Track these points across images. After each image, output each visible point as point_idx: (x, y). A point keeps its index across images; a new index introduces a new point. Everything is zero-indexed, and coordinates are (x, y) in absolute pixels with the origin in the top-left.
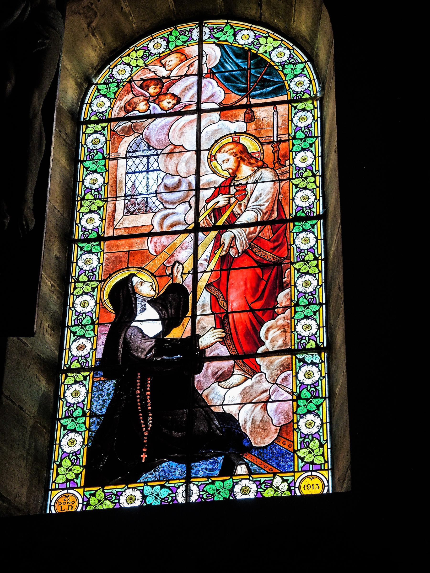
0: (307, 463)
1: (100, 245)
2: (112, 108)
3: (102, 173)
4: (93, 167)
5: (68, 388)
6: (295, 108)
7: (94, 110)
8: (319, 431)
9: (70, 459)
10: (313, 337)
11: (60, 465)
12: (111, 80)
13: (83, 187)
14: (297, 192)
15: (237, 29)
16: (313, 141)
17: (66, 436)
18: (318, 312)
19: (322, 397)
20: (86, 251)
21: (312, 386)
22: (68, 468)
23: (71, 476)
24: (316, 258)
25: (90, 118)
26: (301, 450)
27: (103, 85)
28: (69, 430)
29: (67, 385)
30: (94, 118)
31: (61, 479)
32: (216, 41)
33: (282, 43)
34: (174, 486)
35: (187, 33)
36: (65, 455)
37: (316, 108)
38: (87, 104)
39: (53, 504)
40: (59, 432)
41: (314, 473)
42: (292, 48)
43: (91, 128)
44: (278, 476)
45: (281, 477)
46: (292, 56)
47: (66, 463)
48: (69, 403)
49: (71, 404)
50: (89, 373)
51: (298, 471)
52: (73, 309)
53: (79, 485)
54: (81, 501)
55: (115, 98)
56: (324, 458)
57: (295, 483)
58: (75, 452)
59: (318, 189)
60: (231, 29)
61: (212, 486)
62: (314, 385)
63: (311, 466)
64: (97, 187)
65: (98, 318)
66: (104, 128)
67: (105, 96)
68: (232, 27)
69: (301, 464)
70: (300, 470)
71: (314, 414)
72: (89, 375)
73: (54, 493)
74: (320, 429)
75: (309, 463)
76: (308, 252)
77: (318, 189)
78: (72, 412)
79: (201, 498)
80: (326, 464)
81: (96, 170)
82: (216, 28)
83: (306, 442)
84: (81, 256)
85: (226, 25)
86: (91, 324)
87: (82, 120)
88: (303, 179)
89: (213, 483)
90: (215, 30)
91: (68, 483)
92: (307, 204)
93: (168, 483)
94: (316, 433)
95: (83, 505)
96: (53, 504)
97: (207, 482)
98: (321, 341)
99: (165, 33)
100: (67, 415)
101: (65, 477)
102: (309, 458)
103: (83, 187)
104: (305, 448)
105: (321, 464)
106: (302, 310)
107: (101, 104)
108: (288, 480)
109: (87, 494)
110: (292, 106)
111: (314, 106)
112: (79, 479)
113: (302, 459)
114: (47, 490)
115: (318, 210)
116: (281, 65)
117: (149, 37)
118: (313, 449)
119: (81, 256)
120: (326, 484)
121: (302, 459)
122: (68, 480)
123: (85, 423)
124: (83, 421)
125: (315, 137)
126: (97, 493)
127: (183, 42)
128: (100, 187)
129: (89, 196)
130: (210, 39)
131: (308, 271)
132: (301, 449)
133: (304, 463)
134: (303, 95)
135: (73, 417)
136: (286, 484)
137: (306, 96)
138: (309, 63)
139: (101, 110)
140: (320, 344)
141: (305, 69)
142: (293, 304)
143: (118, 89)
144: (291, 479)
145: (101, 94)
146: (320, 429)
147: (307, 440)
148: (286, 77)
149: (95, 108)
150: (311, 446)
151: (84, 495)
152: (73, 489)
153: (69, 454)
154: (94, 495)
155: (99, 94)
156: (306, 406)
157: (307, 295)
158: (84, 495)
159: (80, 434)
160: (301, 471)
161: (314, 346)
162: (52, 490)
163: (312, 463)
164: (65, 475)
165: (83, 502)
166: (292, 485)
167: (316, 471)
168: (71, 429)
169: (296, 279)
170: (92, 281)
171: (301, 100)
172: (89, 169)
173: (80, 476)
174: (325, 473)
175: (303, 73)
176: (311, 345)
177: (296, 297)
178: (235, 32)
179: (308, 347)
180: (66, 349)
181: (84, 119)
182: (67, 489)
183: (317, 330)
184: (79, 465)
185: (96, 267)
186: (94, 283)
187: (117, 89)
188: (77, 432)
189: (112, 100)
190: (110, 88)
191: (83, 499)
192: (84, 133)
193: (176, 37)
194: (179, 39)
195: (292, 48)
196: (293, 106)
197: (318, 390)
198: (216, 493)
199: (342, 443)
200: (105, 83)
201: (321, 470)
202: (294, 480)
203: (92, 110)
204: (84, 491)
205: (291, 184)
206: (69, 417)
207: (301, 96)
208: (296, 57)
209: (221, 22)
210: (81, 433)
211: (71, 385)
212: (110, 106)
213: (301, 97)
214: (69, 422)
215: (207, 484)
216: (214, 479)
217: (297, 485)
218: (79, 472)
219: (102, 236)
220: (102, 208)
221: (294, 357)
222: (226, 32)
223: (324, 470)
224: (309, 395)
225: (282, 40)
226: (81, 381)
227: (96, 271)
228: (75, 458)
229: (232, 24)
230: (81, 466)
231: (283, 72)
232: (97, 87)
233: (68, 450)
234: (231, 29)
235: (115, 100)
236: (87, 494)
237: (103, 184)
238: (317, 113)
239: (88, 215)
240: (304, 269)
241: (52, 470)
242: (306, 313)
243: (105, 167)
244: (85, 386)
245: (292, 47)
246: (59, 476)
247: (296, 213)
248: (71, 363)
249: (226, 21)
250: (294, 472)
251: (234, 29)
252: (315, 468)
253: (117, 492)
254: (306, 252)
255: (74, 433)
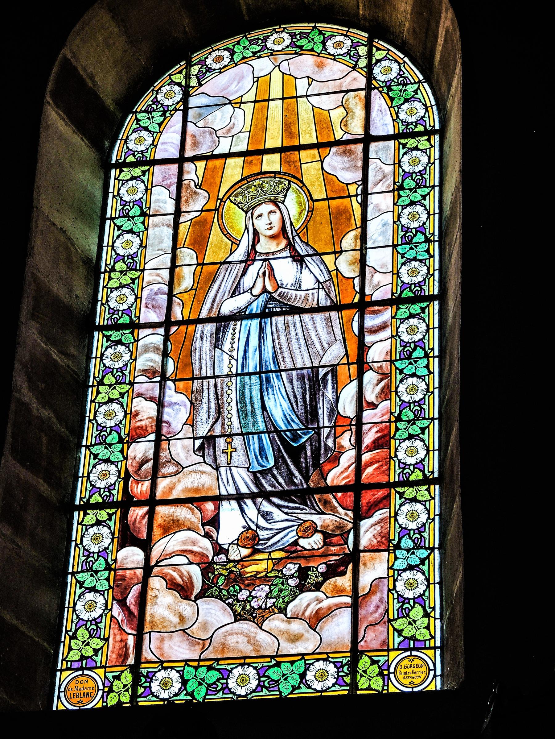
0: (406, 638)
1: (132, 333)
2: (156, 146)
3: (118, 462)
4: (90, 582)
5: (123, 184)
6: (401, 495)
7: (130, 148)
8: (424, 338)
9: (87, 629)
10: (421, 122)
11: (74, 637)
12: (154, 106)
13: (102, 365)
14: (401, 505)
15: (328, 34)
16: (426, 425)
17: (82, 597)
18: (427, 561)
19: (429, 419)
20: (102, 460)
21: (416, 531)
22: (85, 641)
23: (88, 652)
24: (427, 356)
25: (125, 159)
26: (399, 621)
27: (144, 114)
28: (86, 588)
29: (123, 180)
30: (131, 159)
31: (74, 656)
32: (298, 50)
33: (387, 54)
34: (226, 669)
35: (260, 41)
36: (82, 623)
37: (432, 146)
38: (96, 358)
39: (62, 689)
40: (72, 590)
41: (414, 653)
42: (402, 62)
43: (126, 174)
44: (366, 655)
45: (370, 657)
46: (401, 73)
47: (83, 634)
48: (125, 201)
49: (127, 202)
50: (114, 510)
51: (394, 650)
52: (94, 422)
53: (99, 665)
54: (101, 687)
55: (160, 132)
56: (430, 493)
57: (389, 667)
58: (95, 619)
59: (432, 149)
60: (319, 34)
61: (276, 669)
62: (419, 530)
63: (412, 642)
64: (121, 365)
65: (128, 435)
66: (144, 173)
67: (146, 129)
68: (320, 33)
69: (398, 640)
70: (396, 647)
71: (419, 319)
72: (115, 513)
73: (65, 674)
74: (424, 336)
75: (410, 639)
76: (414, 603)
77: (432, 149)
78: (104, 437)
79: (261, 686)
80: (432, 641)
81: (121, 339)
82: (299, 34)
83: (405, 609)
84: (94, 467)
85: (312, 30)
86: (118, 443)
87: (114, 161)
88: (412, 361)
89: (278, 665)
90: (298, 37)
91: (84, 662)
92: (413, 526)
93: (218, 664)
94: (420, 340)
95: (104, 692)
96: (62, 689)
97: (270, 664)
98: (431, 470)
99: (229, 43)
100: (98, 441)
101: (80, 654)
102: (408, 632)
103: (102, 365)
104: (404, 617)
105: (425, 641)
106: (405, 427)
107: (140, 141)
108: (379, 661)
109: (110, 675)
110: (400, 143)
111: (431, 145)
112: (136, 285)
113: (400, 632)
114: (54, 671)
115: (431, 289)
116: (386, 86)
117: (208, 50)
118: (416, 619)
119: (94, 467)
120: (432, 667)
121: (400, 632)
122: (83, 658)
123: (108, 579)
124: (141, 221)
125: (430, 186)
126: (123, 675)
127: (253, 52)
128: (124, 365)
129: (120, 266)
130: (290, 48)
131: (415, 496)
132: (399, 618)
133: (402, 638)
134: (416, 127)
135: (129, 216)
136: (376, 666)
137: (420, 128)
138: (426, 85)
139: (140, 148)
140: (428, 474)
141: (419, 91)
142: (393, 419)
143: (165, 119)
144: (383, 660)
145: (141, 126)
146: (424, 336)
147: (407, 605)
148: (392, 103)
149: (131, 145)
150: (412, 614)
151: (106, 677)
152: (90, 669)
153: (124, 256)
154: (118, 678)
155: (138, 126)
156: (406, 558)
157: (413, 286)
158: (106, 677)
159: (101, 594)
160: (398, 649)
161: (421, 478)
162: (61, 670)
163: (413, 638)
164: (80, 650)
165: (104, 687)
166: (385, 667)
167: (418, 649)
168: (127, 229)
169: (401, 157)
170: (120, 383)
171: (414, 135)
172: (123, 228)
173: (100, 652)
174: (430, 653)
175: (416, 96)
176: (417, 475)
177: (397, 535)
178: (324, 38)
179: (412, 478)
180: (68, 608)
181: (117, 160)
182: (82, 668)
183: (425, 587)
184: (99, 638)
185: (115, 484)
186: (124, 386)
187: (163, 118)
188: (97, 591)
189: (155, 134)
190: (153, 118)
191: (104, 684)
192: (105, 287)
193: (245, 47)
194: (248, 49)
195: (402, 62)
196: (402, 144)
197: (425, 538)
198: (282, 680)
199: (450, 152)
200: (146, 111)
201: (426, 648)
202: (388, 660)
203: (128, 148)
204: (105, 672)
205: (391, 629)
206: (87, 571)
207: (413, 127)
208: (407, 75)
209: (306, 27)
210: (102, 593)
211: (127, 181)
212: (153, 144)
213: (413, 130)
214: (101, 450)
215: (270, 667)
216: (279, 659)
217: (392, 670)
218: (99, 646)
219: (137, 322)
220: (126, 395)
221: (393, 491)
222: (313, 39)
223: (430, 648)
224: (411, 544)
225: (389, 50)
226: (139, 177)
227: (114, 489)
228: (95, 627)
229: (320, 29)
230: (101, 639)
231: (388, 94)
232: (136, 116)
233: (85, 616)
234: (319, 34)
235: (159, 134)
236: (110, 675)
237: (128, 361)
238: (436, 153)
239: (94, 530)
240: (410, 254)
241: (62, 644)
242: (412, 198)
243: (144, 225)
244: (143, 182)
245: (402, 59)
246: (100, 395)
247: (401, 292)
248: (90, 497)
249: (313, 25)
250: (389, 650)
251: (324, 35)
252: (418, 645)
253: (148, 672)
254: (412, 602)
255: (130, 234)
